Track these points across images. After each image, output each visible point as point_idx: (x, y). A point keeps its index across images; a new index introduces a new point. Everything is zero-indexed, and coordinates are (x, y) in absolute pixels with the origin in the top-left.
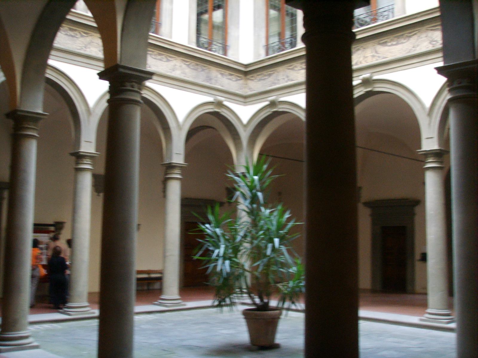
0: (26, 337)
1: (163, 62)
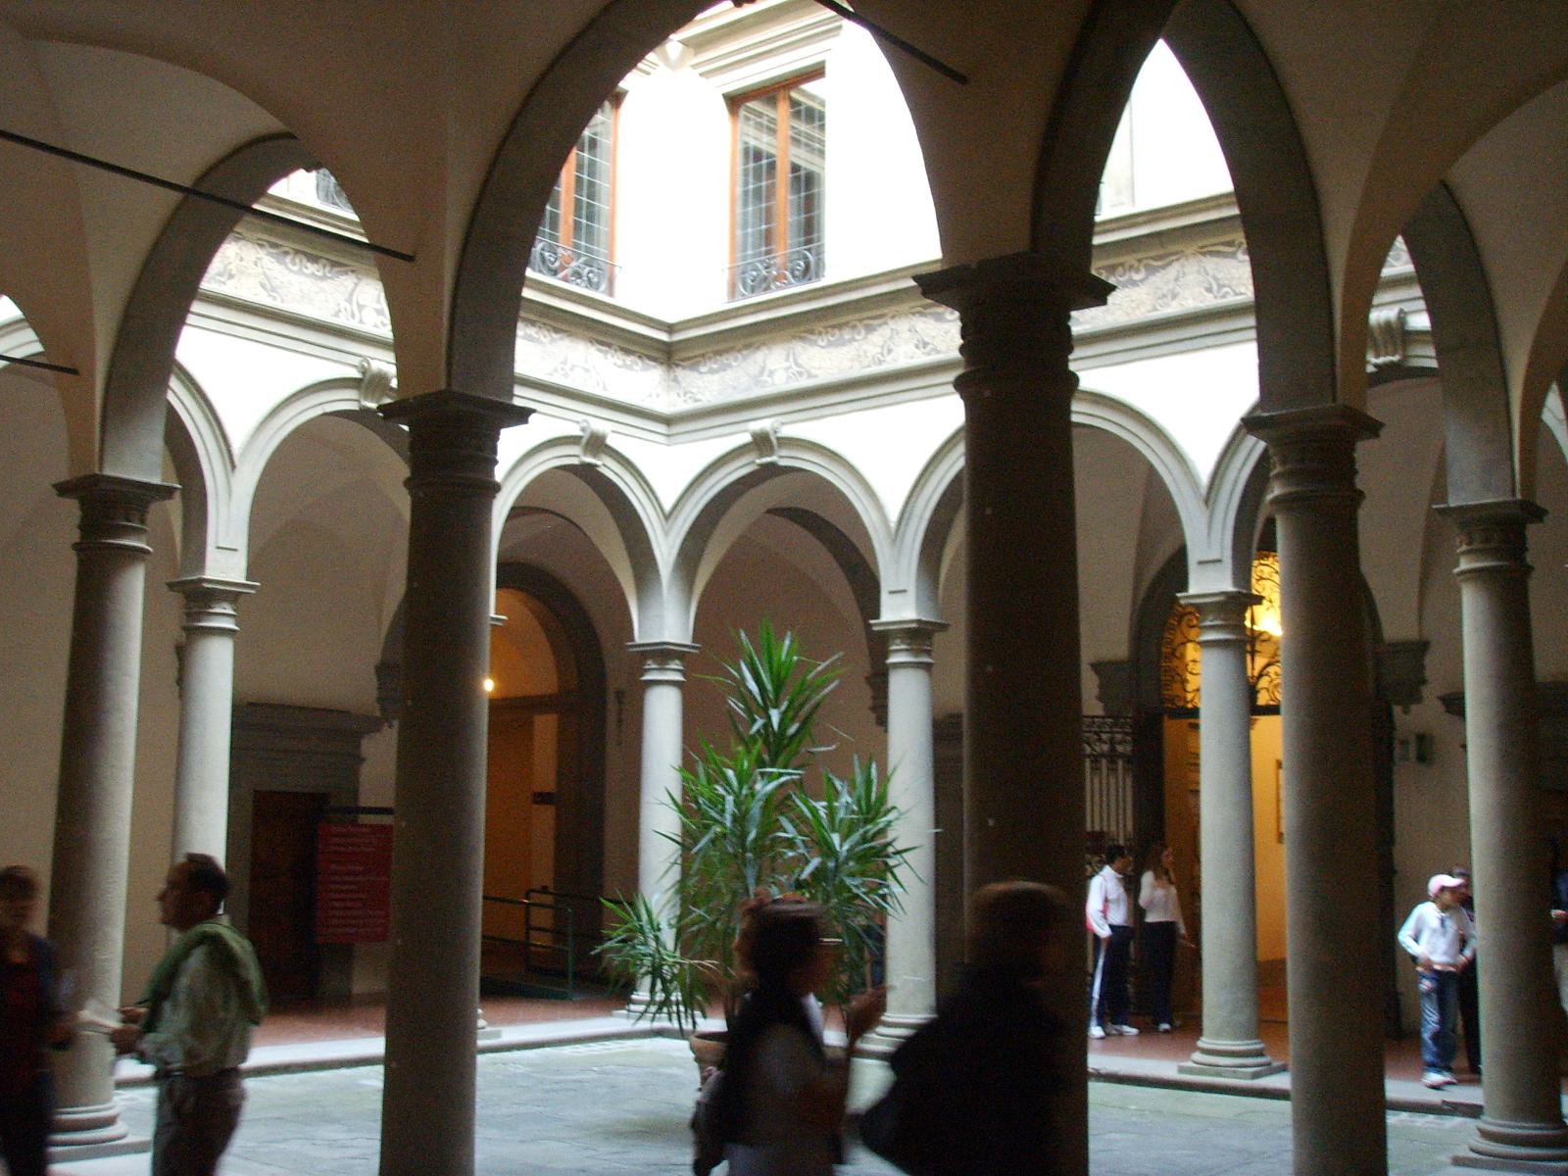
0: (109, 1122)
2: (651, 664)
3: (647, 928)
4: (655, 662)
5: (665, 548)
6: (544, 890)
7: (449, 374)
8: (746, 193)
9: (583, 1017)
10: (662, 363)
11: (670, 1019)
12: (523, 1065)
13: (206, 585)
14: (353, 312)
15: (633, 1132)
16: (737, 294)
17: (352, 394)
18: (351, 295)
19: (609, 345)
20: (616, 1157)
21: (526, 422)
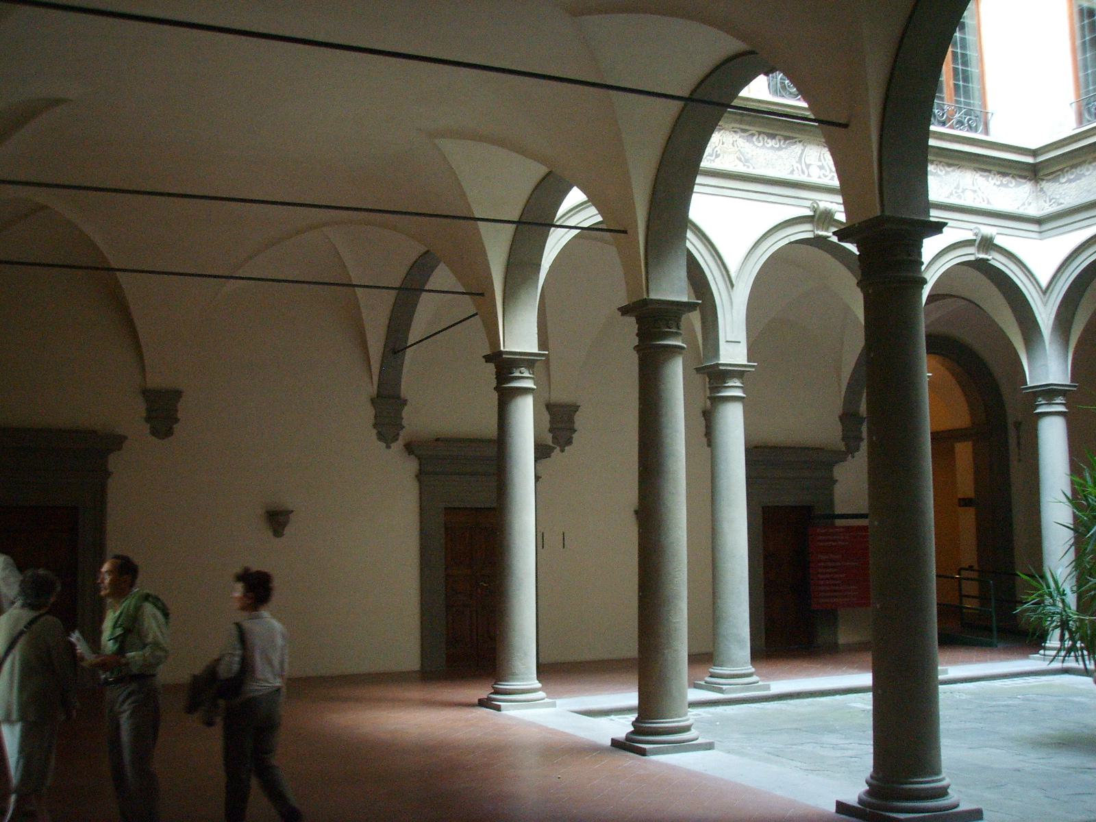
0: (687, 729)
1: (1010, 189)
2: (1041, 401)
3: (1055, 594)
4: (1044, 399)
5: (1045, 314)
6: (971, 568)
7: (882, 205)
8: (1084, 43)
9: (1007, 660)
10: (1030, 180)
11: (1077, 661)
12: (966, 694)
13: (721, 368)
14: (802, 170)
15: (1051, 744)
16: (1084, 120)
17: (808, 227)
18: (800, 157)
19: (989, 171)
20: (1042, 761)
21: (941, 232)
